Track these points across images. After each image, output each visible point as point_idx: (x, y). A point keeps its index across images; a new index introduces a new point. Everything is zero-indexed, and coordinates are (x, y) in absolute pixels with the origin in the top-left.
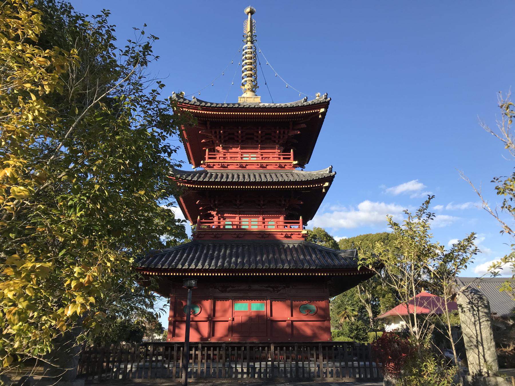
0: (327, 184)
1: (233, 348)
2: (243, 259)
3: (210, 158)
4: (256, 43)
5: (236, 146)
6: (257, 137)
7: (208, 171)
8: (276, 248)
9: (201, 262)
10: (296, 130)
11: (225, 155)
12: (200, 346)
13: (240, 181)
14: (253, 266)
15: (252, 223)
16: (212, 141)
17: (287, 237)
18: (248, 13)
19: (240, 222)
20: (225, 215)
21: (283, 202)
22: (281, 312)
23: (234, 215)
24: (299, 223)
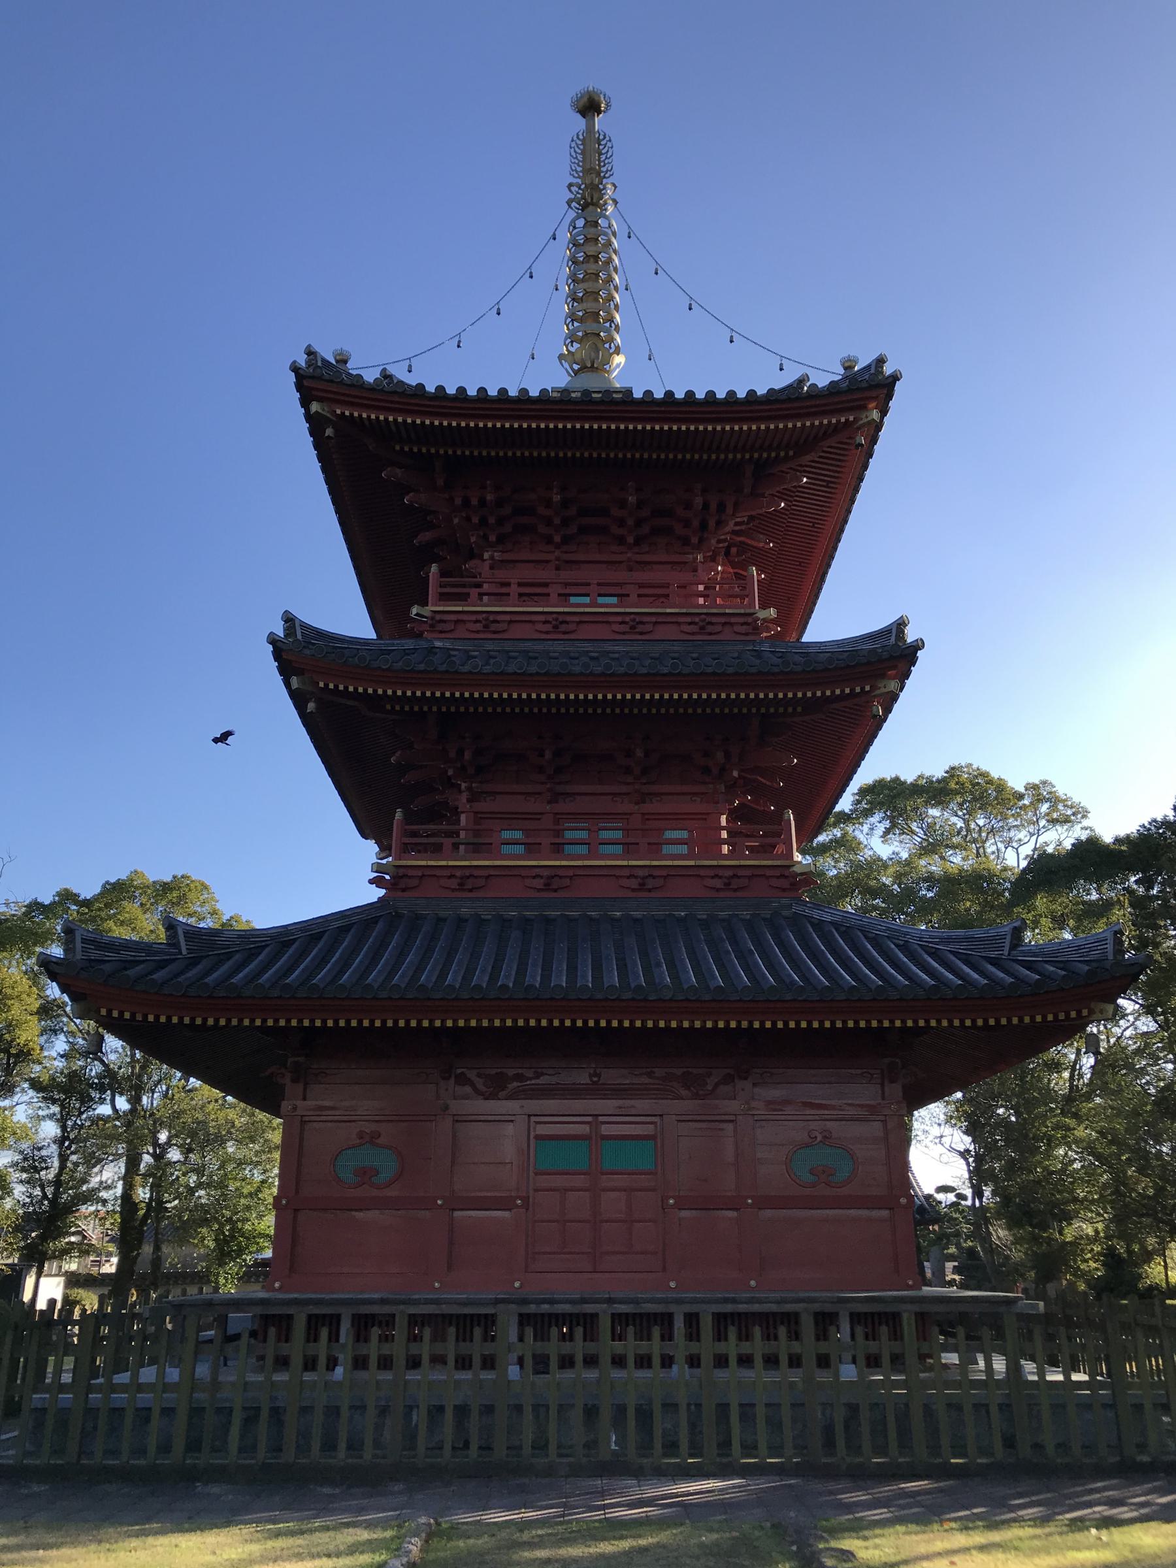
15: (604, 835)
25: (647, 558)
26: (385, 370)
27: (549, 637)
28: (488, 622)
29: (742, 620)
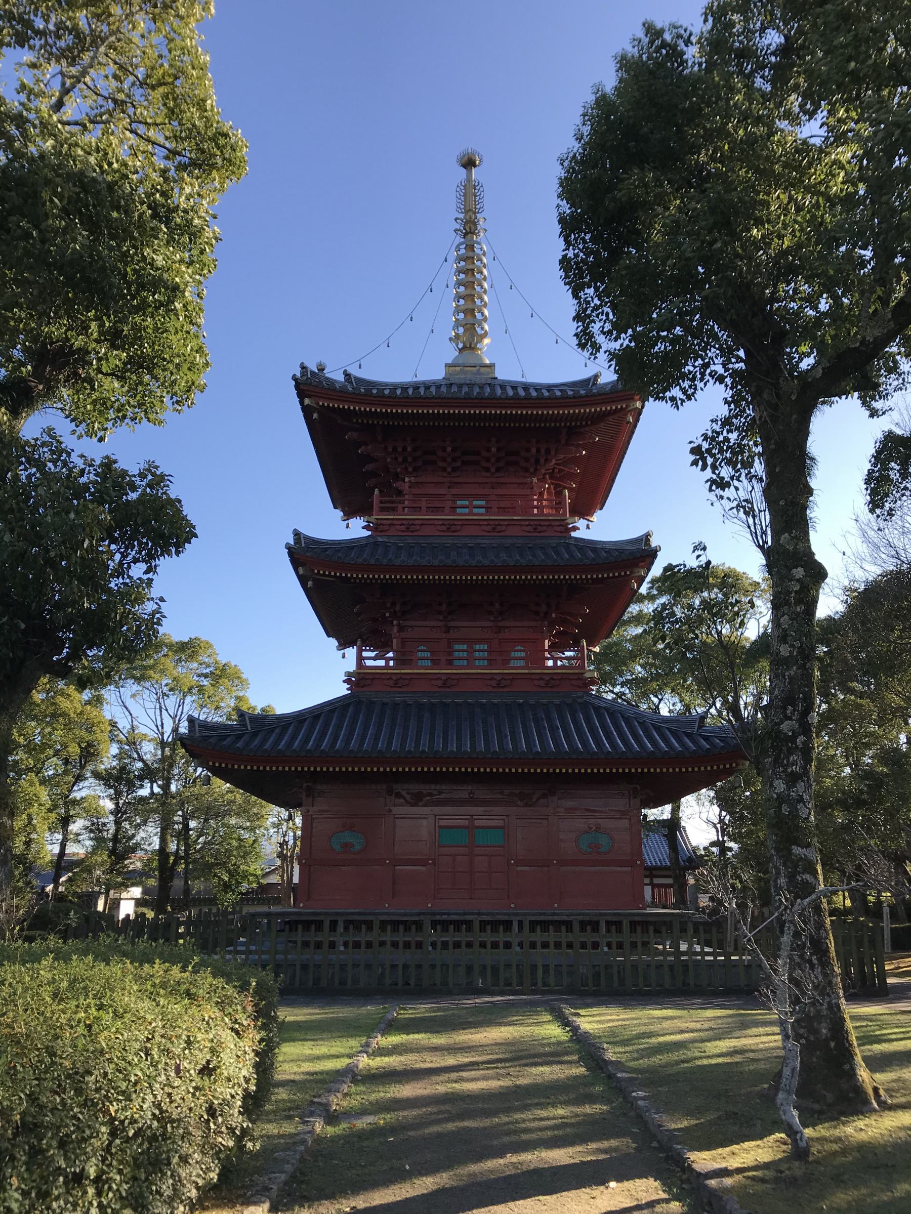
21: (544, 608)
25: (502, 480)
26: (345, 371)
27: (446, 534)
28: (409, 526)
29: (558, 523)
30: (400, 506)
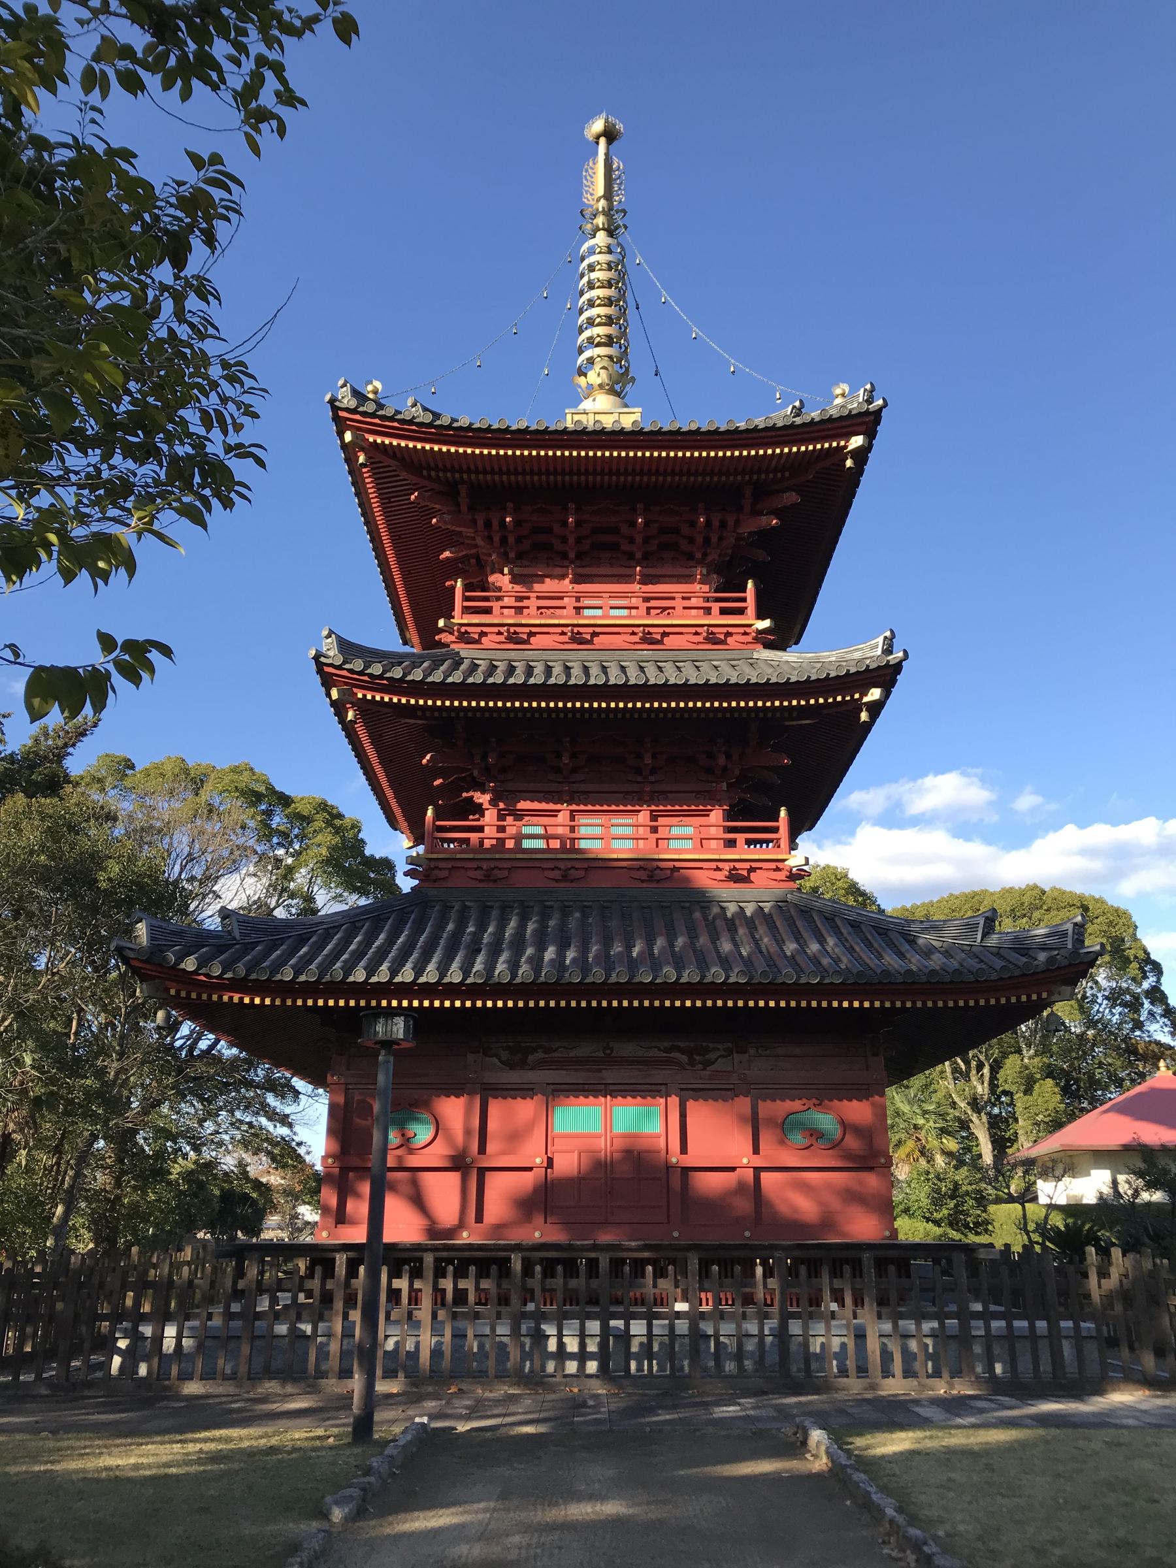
0: (875, 694)
1: (549, 1269)
2: (584, 950)
3: (466, 610)
4: (626, 237)
5: (558, 571)
6: (632, 541)
7: (463, 654)
8: (697, 915)
9: (435, 960)
10: (763, 513)
11: (520, 599)
12: (429, 1259)
13: (572, 681)
14: (619, 976)
15: (615, 831)
16: (478, 558)
17: (735, 877)
18: (598, 137)
19: (573, 829)
20: (522, 805)
21: (722, 761)
22: (714, 1142)
23: (551, 806)
24: (775, 830)
30: (496, 606)
